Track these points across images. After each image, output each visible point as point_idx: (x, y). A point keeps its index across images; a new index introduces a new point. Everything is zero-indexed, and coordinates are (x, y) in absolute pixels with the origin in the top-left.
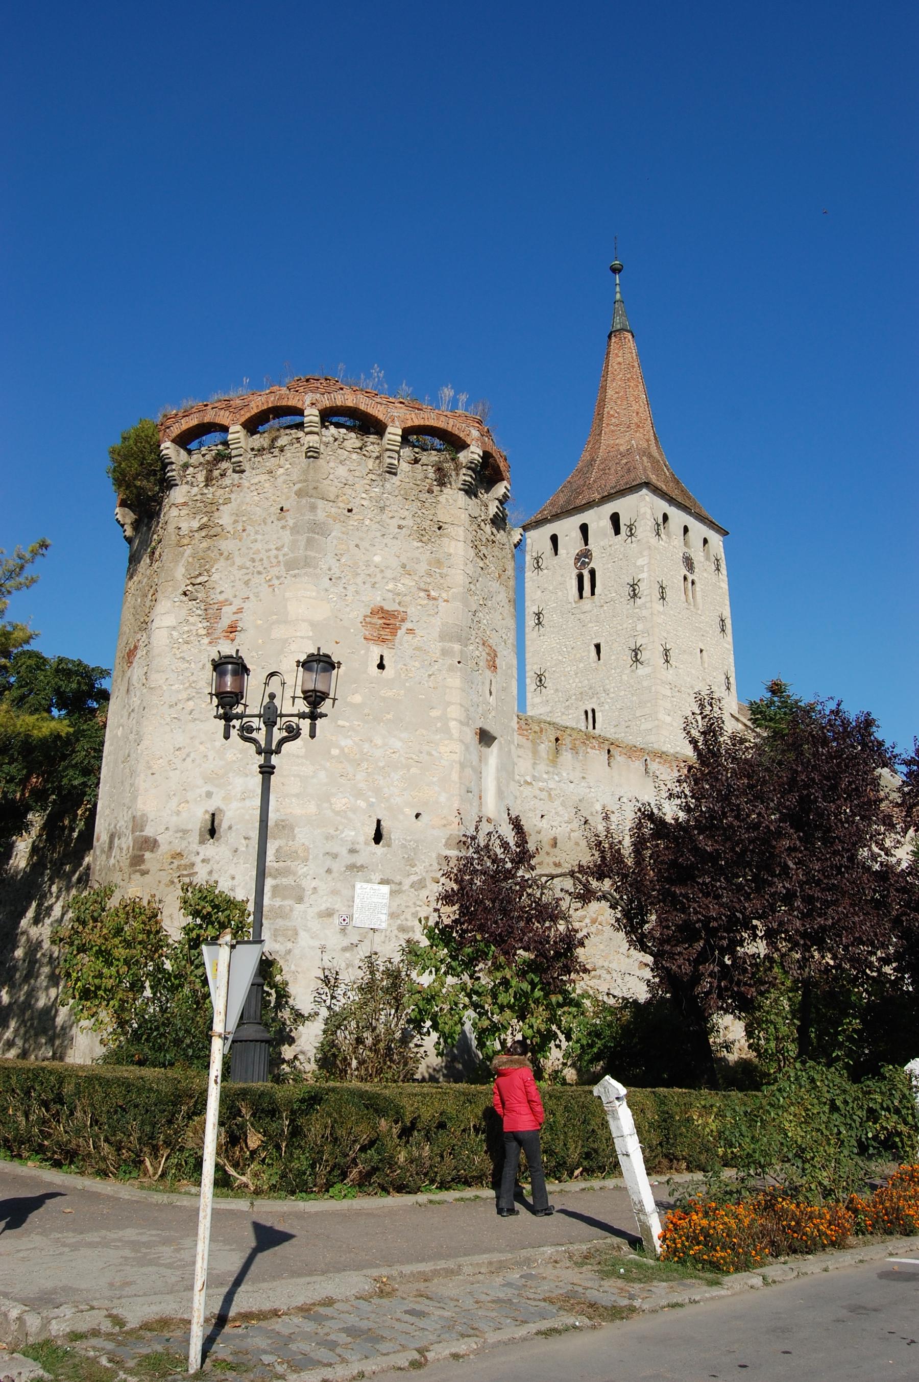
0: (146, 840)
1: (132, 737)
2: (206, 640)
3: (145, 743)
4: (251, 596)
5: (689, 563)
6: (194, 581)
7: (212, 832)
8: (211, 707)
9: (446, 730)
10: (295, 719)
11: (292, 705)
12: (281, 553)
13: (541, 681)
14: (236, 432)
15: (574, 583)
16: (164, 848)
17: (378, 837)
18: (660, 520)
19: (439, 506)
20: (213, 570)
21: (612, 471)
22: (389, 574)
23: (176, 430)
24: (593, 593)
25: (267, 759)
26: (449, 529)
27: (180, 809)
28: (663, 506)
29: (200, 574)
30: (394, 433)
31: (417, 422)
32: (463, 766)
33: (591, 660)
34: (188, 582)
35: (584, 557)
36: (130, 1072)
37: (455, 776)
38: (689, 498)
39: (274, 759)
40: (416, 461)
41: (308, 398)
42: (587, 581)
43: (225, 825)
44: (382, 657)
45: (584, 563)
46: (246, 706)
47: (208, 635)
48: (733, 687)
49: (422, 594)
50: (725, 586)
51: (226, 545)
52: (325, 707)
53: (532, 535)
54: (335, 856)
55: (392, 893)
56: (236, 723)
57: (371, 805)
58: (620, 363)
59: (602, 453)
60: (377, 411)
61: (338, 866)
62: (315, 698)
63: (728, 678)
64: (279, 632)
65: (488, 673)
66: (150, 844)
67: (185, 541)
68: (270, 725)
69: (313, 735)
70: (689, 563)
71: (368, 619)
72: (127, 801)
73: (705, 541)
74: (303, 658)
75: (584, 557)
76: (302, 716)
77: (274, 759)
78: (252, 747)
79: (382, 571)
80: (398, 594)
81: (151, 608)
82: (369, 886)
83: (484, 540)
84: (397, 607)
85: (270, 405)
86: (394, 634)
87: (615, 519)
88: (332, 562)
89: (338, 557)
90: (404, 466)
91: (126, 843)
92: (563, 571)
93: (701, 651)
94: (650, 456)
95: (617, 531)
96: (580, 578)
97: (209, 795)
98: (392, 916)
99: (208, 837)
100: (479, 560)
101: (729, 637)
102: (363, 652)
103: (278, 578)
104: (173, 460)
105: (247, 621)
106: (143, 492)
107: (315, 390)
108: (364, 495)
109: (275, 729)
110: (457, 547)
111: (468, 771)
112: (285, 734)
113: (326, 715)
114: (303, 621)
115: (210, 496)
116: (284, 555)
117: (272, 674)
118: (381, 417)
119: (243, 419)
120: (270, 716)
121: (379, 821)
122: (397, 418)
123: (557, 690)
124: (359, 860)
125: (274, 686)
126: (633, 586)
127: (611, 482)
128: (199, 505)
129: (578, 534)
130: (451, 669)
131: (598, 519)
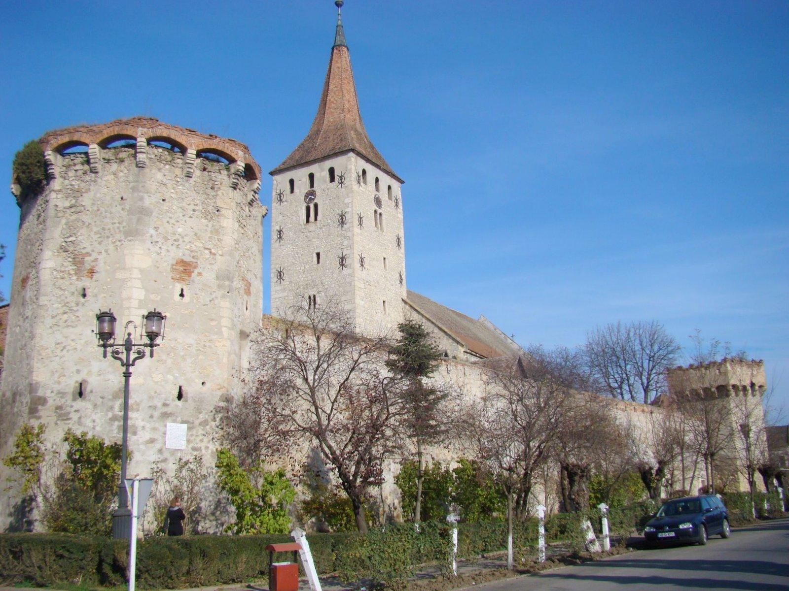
0: (40, 398)
1: (27, 334)
2: (75, 278)
3: (37, 339)
4: (103, 251)
5: (378, 202)
6: (66, 240)
7: (81, 394)
8: (95, 340)
9: (220, 333)
10: (142, 347)
11: (139, 337)
12: (121, 226)
13: (280, 275)
14: (94, 149)
15: (304, 212)
16: (51, 402)
17: (180, 396)
18: (361, 174)
19: (218, 197)
20: (79, 234)
21: (331, 138)
22: (187, 239)
23: (56, 142)
24: (316, 219)
25: (127, 369)
26: (223, 212)
27: (60, 380)
28: (362, 164)
29: (71, 236)
30: (192, 152)
31: (207, 146)
32: (229, 354)
33: (313, 263)
34: (63, 240)
35: (310, 195)
36: (11, 534)
37: (225, 360)
38: (380, 158)
39: (131, 369)
40: (205, 169)
41: (140, 130)
42: (312, 212)
43: (88, 389)
44: (182, 290)
45: (311, 200)
46: (115, 339)
47: (76, 274)
48: (404, 282)
49: (207, 252)
50: (401, 216)
51: (86, 218)
52: (158, 341)
53: (278, 178)
54: (155, 408)
55: (189, 429)
56: (109, 350)
57: (176, 378)
58: (338, 67)
59: (325, 127)
60: (182, 139)
61: (156, 414)
62: (152, 336)
63: (401, 276)
64: (120, 275)
65: (245, 296)
66: (43, 401)
67: (60, 214)
68: (128, 350)
69: (152, 355)
70: (378, 202)
71: (174, 267)
72: (25, 374)
73: (389, 187)
74: (146, 314)
75: (310, 195)
76: (146, 345)
77: (131, 369)
78: (119, 363)
79: (183, 237)
80: (192, 251)
81: (38, 255)
82: (175, 424)
83: (244, 216)
84: (192, 259)
85: (116, 133)
86: (190, 276)
87: (332, 171)
88: (152, 231)
89: (156, 228)
90: (198, 173)
91: (26, 399)
92: (297, 204)
93: (384, 259)
94: (356, 130)
95: (332, 179)
96: (308, 209)
97: (78, 371)
98: (188, 441)
99: (78, 396)
100: (240, 229)
101: (403, 250)
102: (171, 287)
103: (119, 241)
104: (53, 162)
105: (101, 267)
106: (32, 182)
107: (143, 126)
108: (173, 191)
109: (131, 352)
110: (228, 222)
111: (233, 356)
112: (137, 355)
113: (158, 345)
114: (135, 268)
115: (76, 187)
116: (124, 227)
117: (130, 322)
118: (184, 143)
119: (98, 141)
120: (128, 345)
121: (180, 387)
122: (193, 145)
123: (291, 282)
124: (169, 410)
125: (131, 329)
126: (342, 216)
127: (329, 147)
128: (69, 192)
129: (307, 180)
130: (223, 296)
131: (320, 171)
